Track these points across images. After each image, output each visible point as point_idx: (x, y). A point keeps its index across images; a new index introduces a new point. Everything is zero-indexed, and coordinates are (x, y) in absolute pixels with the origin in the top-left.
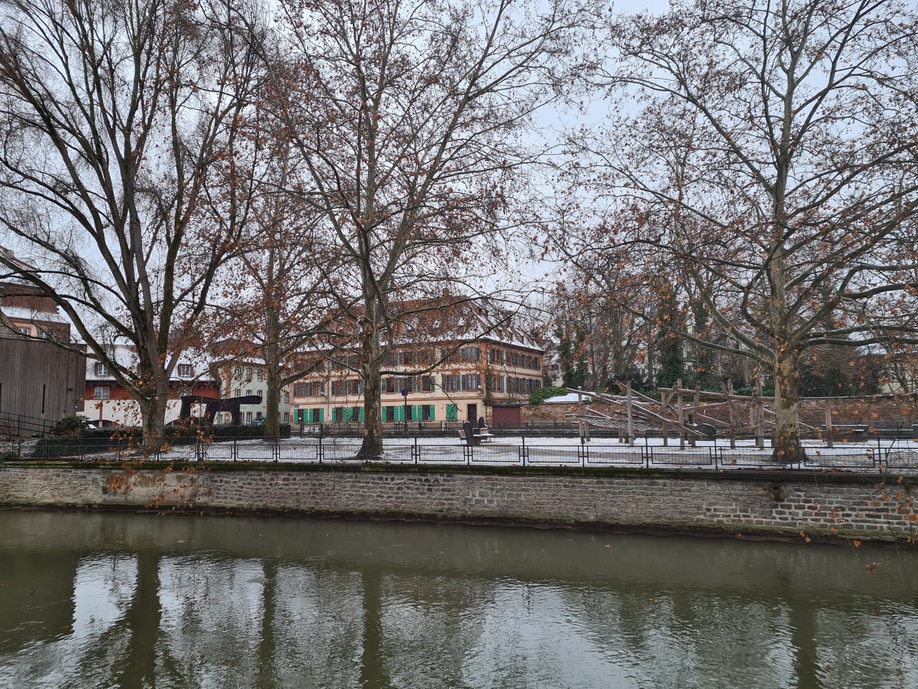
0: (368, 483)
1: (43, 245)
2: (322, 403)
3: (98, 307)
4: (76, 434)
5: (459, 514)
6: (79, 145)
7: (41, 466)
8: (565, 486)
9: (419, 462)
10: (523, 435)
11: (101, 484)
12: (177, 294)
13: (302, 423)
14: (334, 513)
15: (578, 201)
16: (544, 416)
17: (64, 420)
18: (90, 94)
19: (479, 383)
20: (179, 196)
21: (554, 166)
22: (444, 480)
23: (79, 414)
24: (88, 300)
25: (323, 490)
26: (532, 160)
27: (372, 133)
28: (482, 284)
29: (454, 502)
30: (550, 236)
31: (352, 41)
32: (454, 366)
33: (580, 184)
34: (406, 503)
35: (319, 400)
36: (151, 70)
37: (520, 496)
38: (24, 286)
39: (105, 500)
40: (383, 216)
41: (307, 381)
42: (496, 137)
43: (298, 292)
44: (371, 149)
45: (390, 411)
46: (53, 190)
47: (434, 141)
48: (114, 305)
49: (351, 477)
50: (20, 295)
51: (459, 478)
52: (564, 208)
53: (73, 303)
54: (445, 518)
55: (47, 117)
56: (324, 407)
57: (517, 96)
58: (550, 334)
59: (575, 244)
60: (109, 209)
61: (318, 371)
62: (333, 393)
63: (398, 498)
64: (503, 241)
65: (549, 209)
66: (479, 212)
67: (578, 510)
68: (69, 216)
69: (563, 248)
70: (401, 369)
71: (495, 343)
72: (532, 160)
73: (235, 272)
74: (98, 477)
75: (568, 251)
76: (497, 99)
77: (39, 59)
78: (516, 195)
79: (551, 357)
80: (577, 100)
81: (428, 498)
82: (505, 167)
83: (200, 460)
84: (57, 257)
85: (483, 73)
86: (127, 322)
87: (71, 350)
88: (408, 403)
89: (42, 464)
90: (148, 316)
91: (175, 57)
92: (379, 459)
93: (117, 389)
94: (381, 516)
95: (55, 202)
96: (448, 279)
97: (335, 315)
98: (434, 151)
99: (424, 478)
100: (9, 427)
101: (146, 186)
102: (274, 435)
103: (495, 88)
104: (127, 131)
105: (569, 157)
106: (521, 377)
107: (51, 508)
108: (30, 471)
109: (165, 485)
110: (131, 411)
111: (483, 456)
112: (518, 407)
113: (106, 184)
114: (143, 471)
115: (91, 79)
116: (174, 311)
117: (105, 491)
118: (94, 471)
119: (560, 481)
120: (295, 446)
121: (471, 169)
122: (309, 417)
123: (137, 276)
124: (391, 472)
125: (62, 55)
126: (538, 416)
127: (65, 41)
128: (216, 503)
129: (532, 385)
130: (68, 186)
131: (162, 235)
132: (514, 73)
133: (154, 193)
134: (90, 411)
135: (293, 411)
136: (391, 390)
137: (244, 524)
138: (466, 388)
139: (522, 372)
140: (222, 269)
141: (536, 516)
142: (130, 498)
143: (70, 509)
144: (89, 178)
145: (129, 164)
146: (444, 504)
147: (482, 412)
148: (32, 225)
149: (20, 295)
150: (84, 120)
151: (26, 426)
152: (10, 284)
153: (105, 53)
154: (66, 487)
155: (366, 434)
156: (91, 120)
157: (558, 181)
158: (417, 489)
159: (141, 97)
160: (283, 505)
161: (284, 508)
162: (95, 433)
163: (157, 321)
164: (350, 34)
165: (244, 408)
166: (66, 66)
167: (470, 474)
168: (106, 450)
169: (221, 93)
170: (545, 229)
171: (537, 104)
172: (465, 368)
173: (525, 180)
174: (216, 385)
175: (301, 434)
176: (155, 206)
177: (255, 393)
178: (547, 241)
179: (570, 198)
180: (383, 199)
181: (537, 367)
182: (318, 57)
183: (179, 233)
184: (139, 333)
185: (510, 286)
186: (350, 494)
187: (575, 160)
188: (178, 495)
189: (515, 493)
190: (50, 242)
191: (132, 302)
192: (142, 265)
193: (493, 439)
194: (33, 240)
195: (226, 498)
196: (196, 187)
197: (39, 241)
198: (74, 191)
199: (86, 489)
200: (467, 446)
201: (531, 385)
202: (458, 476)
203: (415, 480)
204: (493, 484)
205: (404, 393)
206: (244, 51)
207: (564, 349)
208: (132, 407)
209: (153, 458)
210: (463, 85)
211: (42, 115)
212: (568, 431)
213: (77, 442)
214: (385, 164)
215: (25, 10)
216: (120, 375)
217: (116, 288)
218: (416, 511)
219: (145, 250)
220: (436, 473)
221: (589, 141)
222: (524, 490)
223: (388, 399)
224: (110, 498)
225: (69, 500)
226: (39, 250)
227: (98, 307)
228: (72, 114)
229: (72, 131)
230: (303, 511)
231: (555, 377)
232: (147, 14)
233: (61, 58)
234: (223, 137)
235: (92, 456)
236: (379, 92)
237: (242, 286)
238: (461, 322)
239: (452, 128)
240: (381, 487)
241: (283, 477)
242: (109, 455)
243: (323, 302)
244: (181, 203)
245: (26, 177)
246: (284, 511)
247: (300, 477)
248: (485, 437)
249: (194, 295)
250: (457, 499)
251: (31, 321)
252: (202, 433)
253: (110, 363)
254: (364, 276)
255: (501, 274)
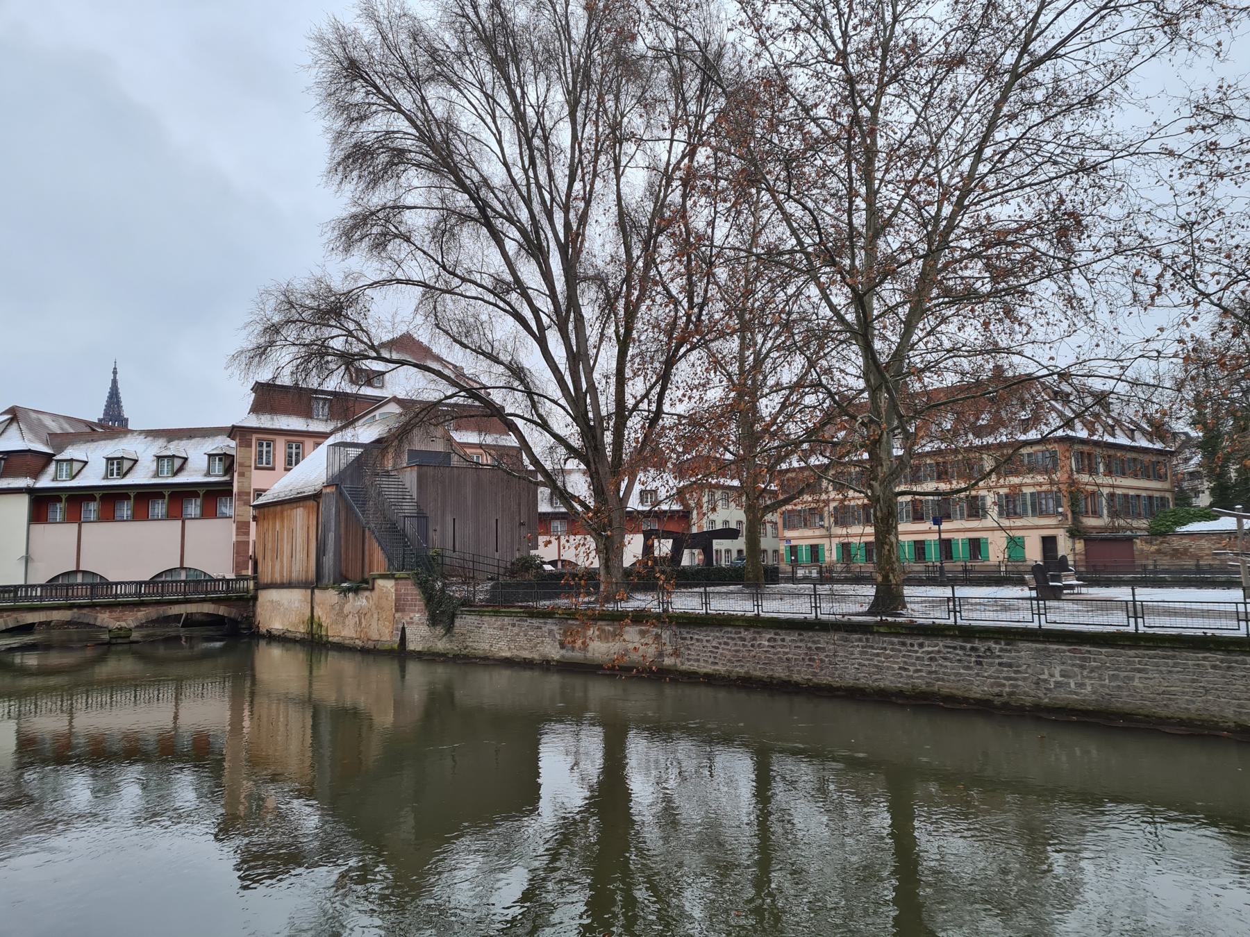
0: (885, 649)
1: (487, 358)
2: (822, 537)
3: (544, 426)
4: (530, 576)
5: (1028, 701)
6: (517, 235)
7: (496, 614)
8: (1214, 667)
9: (959, 622)
10: (1133, 584)
11: (558, 637)
12: (630, 402)
13: (795, 564)
14: (839, 689)
15: (1220, 205)
16: (1176, 553)
17: (517, 560)
18: (526, 171)
19: (1059, 504)
20: (627, 280)
21: (1171, 153)
22: (1001, 650)
23: (533, 552)
24: (536, 418)
25: (822, 656)
26: (1131, 151)
27: (871, 153)
28: (1053, 353)
29: (1020, 683)
30: (1166, 267)
31: (837, 33)
32: (1015, 480)
33: (1222, 176)
34: (943, 680)
35: (818, 532)
36: (590, 130)
37: (1132, 679)
38: (470, 406)
39: (563, 656)
40: (889, 268)
41: (799, 508)
42: (1068, 125)
43: (778, 387)
44: (868, 178)
45: (920, 547)
46: (491, 292)
47: (966, 150)
48: (562, 422)
49: (860, 640)
50: (466, 417)
51: (1025, 651)
52: (1193, 218)
53: (520, 423)
54: (1006, 706)
55: (483, 206)
56: (825, 542)
57: (1102, 57)
58: (1180, 426)
59: (1213, 275)
60: (552, 308)
61: (812, 493)
62: (836, 523)
63: (930, 673)
64: (1086, 285)
65: (1166, 225)
66: (1043, 246)
67: (1240, 706)
68: (510, 320)
69: (1193, 280)
70: (930, 486)
71: (1082, 441)
72: (1131, 151)
73: (699, 369)
74: (554, 627)
75: (1201, 286)
76: (1066, 67)
77: (473, 141)
78: (1103, 210)
79: (1187, 460)
80: (1211, 41)
81: (978, 675)
82: (1083, 168)
83: (666, 611)
84: (501, 369)
85: (1038, 35)
86: (576, 442)
87: (519, 478)
88: (944, 536)
89: (497, 612)
90: (599, 431)
91: (617, 107)
92: (900, 615)
93: (572, 521)
94: (908, 698)
95: (495, 305)
96: (997, 350)
97: (828, 419)
98: (966, 164)
99: (969, 646)
100: (464, 568)
101: (591, 272)
102: (758, 580)
103: (1062, 51)
104: (566, 209)
105: (1199, 135)
106: (1132, 493)
107: (509, 663)
108: (486, 619)
109: (624, 640)
110: (582, 549)
111: (1063, 615)
112: (1130, 540)
113: (547, 275)
114: (600, 623)
115: (526, 153)
116: (629, 424)
117: (562, 646)
118: (550, 621)
119: (1205, 659)
120: (782, 596)
121: (1027, 180)
122: (804, 556)
123: (584, 386)
124: (919, 635)
125: (495, 131)
126: (1165, 554)
127: (497, 114)
128: (686, 666)
129: (1153, 506)
130: (508, 284)
131: (611, 331)
132: (1092, 22)
133: (600, 280)
134: (547, 551)
135: (783, 547)
136: (918, 517)
137: (722, 695)
138: (1038, 511)
139: (1128, 484)
140: (682, 365)
141: (1164, 713)
142: (589, 655)
143: (527, 664)
144: (530, 273)
145: (572, 246)
146: (1004, 685)
147: (1064, 546)
148: (475, 336)
149: (466, 417)
150: (522, 204)
151: (481, 567)
152: (456, 405)
153: (539, 121)
154: (522, 639)
155: (880, 579)
156: (528, 202)
157: (1181, 176)
158: (959, 661)
159: (580, 161)
160: (770, 673)
161: (771, 677)
162: (551, 574)
163: (608, 437)
164: (834, 23)
165: (718, 544)
166: (500, 142)
167: (1043, 642)
168: (557, 596)
169: (672, 140)
170: (1157, 256)
171: (1137, 60)
172: (1030, 484)
173: (1119, 185)
174: (685, 515)
175: (793, 579)
176: (602, 296)
177: (733, 525)
178: (1161, 276)
179: (1206, 202)
180: (891, 242)
181: (1160, 478)
182: (789, 65)
183: (629, 330)
184: (590, 454)
185: (1101, 352)
186: (859, 664)
187: (1211, 137)
188: (640, 653)
189: (1122, 674)
190: (494, 354)
191: (580, 417)
192: (590, 371)
193: (1084, 590)
194: (478, 353)
195: (698, 660)
196: (647, 267)
197: (483, 353)
198: (514, 290)
199: (543, 642)
200: (1037, 599)
201: (1151, 505)
202: (1021, 645)
203: (955, 648)
204: (1084, 659)
205: (937, 521)
206: (698, 81)
207: (1209, 445)
208: (584, 545)
209: (610, 607)
210: (1009, 59)
211: (477, 206)
212: (1223, 577)
213: (531, 586)
214: (889, 195)
215: (456, 86)
216: (572, 507)
217: (563, 402)
218: (959, 693)
219: (592, 352)
220: (988, 639)
221: (1234, 104)
222: (1140, 671)
223: (908, 531)
224: (568, 654)
225: (526, 654)
226: (484, 363)
227: (544, 426)
228: (509, 199)
229: (510, 220)
230: (797, 684)
231: (1197, 493)
232: (582, 60)
233: (495, 135)
234: (675, 197)
235: (547, 603)
236: (880, 92)
237: (705, 386)
238: (1023, 415)
239: (992, 126)
240: (904, 656)
241: (768, 636)
242: (563, 602)
243: (810, 400)
244: (630, 288)
245: (464, 280)
246: (771, 682)
247: (790, 637)
248: (1071, 587)
249: (650, 402)
250: (1025, 679)
251: (480, 446)
252: (663, 577)
253: (560, 491)
254: (866, 358)
255: (1083, 336)
